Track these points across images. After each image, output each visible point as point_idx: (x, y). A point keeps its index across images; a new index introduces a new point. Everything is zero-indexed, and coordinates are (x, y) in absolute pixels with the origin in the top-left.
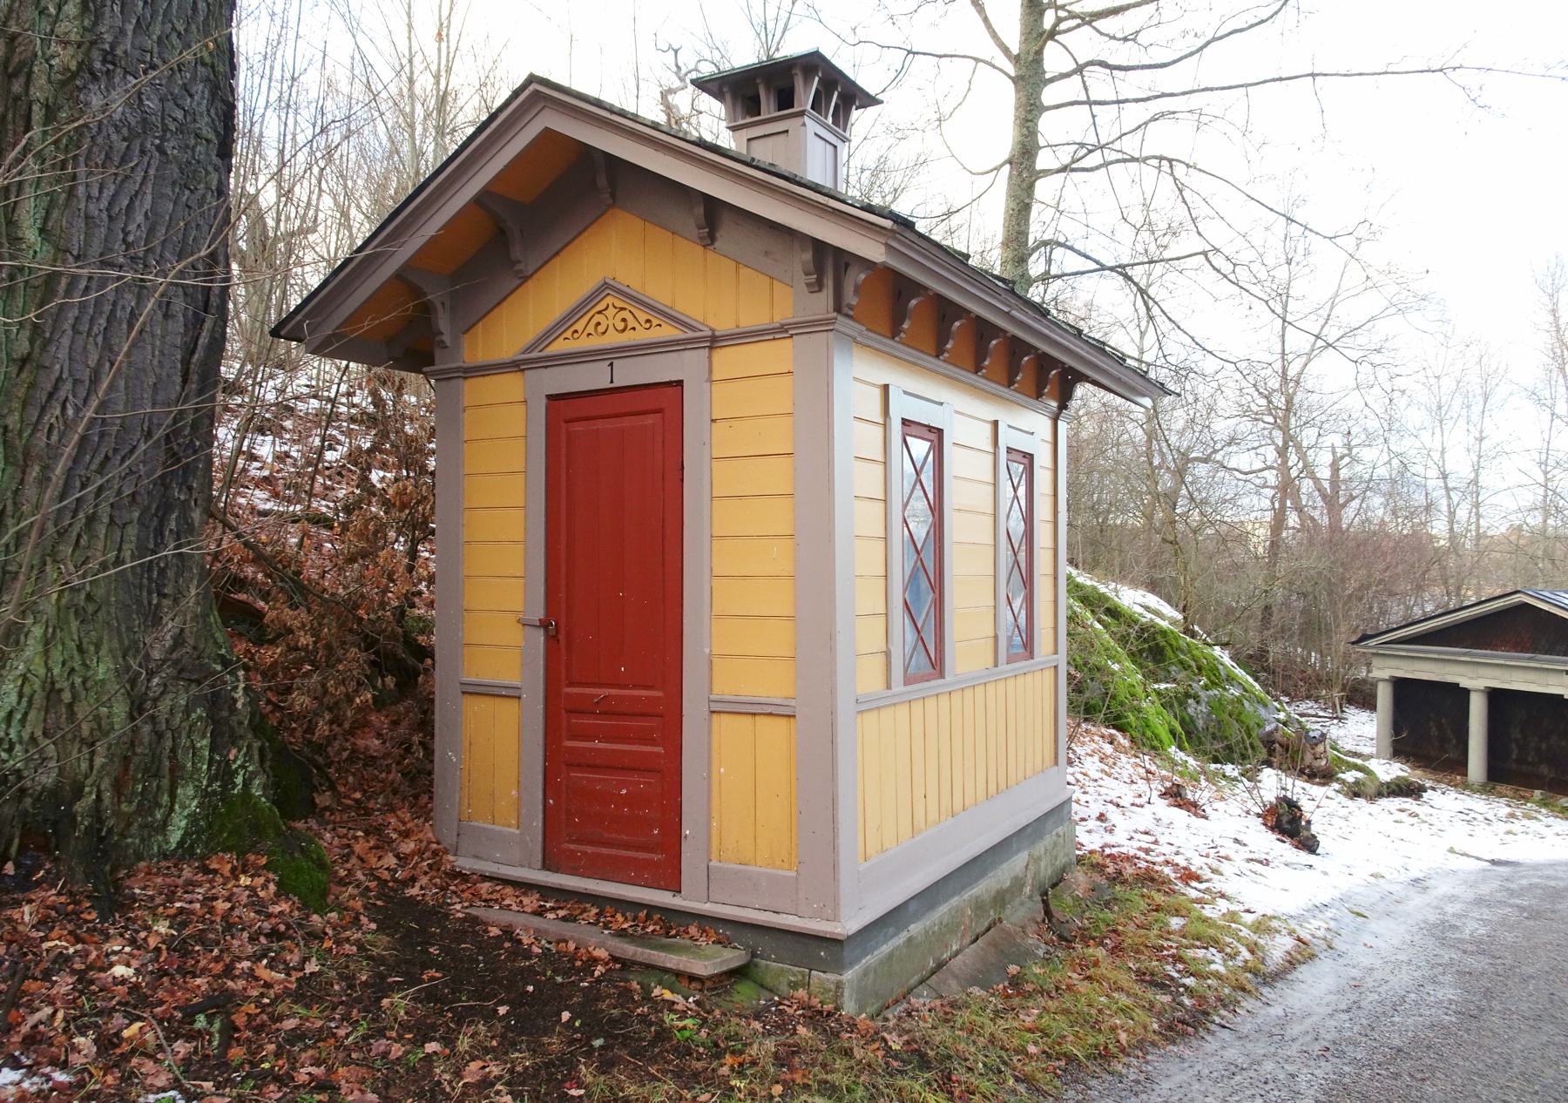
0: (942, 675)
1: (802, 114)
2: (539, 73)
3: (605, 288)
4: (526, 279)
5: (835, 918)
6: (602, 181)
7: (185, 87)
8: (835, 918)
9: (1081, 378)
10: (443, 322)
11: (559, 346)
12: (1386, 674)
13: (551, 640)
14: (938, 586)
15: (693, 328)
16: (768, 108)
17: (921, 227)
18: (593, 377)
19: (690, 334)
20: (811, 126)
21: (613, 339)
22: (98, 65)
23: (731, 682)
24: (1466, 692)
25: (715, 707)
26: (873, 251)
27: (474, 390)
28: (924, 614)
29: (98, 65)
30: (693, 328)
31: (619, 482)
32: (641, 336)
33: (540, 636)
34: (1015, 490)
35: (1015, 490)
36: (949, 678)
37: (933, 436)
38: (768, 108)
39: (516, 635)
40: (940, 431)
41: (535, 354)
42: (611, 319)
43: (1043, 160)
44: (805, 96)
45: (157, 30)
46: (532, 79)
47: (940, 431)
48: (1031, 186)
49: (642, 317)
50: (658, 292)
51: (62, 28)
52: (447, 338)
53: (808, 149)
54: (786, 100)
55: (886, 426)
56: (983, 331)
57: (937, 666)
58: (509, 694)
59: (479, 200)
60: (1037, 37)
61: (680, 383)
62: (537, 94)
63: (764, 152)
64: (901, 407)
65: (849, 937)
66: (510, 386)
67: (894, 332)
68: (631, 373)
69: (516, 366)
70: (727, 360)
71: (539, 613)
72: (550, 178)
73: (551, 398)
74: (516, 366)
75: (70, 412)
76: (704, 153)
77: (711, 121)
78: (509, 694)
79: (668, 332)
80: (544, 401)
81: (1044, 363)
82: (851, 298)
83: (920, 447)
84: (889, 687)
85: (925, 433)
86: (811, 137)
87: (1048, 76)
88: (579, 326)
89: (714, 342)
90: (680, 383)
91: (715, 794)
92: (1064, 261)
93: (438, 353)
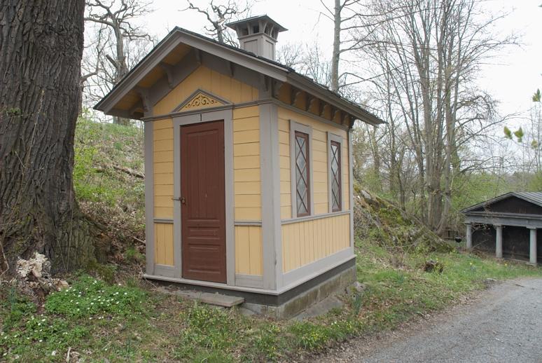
0: (310, 214)
1: (262, 34)
2: (180, 26)
3: (199, 91)
4: (173, 89)
5: (275, 290)
6: (198, 57)
7: (71, 36)
8: (275, 290)
9: (356, 118)
10: (146, 103)
11: (184, 110)
12: (500, 224)
13: (183, 204)
14: (308, 185)
15: (227, 103)
16: (251, 32)
17: (296, 71)
18: (195, 119)
19: (226, 105)
20: (265, 38)
21: (201, 107)
22: (48, 31)
23: (241, 217)
24: (529, 230)
25: (236, 224)
26: (284, 79)
27: (157, 124)
28: (303, 193)
29: (48, 31)
30: (227, 103)
31: (203, 154)
32: (211, 106)
33: (179, 204)
34: (334, 154)
35: (334, 154)
36: (312, 215)
37: (306, 136)
38: (251, 32)
39: (170, 203)
40: (308, 135)
41: (176, 112)
42: (201, 101)
43: (341, 47)
44: (262, 29)
45: (64, 20)
46: (176, 28)
47: (308, 135)
48: (339, 55)
49: (211, 100)
50: (216, 93)
51: (38, 21)
52: (148, 108)
53: (263, 47)
54: (256, 30)
55: (327, 142)
56: (321, 104)
57: (308, 211)
58: (169, 223)
59: (161, 63)
60: (339, 9)
61: (223, 120)
62: (178, 33)
63: (249, 48)
64: (294, 127)
65: (280, 295)
66: (168, 123)
67: (292, 103)
68: (207, 118)
69: (170, 116)
70: (238, 113)
71: (178, 195)
72: (182, 57)
73: (182, 126)
74: (170, 116)
75: (38, 134)
76: (231, 50)
77: (232, 37)
78: (169, 223)
79: (219, 104)
80: (179, 127)
81: (343, 113)
82: (277, 93)
83: (335, 148)
84: (292, 217)
85: (303, 136)
86: (265, 43)
87: (341, 20)
88: (190, 103)
89: (234, 107)
90: (223, 120)
91: (237, 264)
92: (350, 79)
93: (145, 113)
